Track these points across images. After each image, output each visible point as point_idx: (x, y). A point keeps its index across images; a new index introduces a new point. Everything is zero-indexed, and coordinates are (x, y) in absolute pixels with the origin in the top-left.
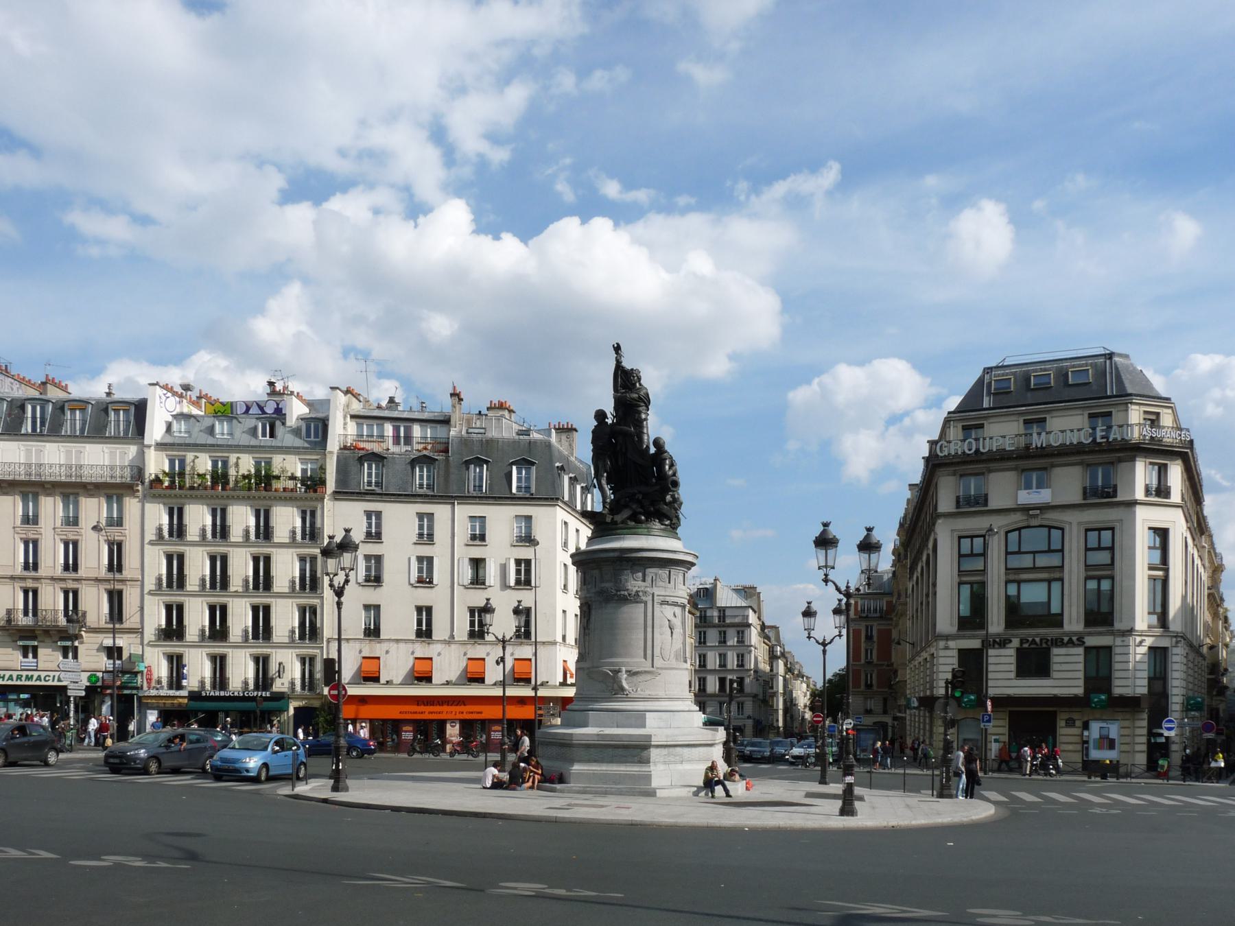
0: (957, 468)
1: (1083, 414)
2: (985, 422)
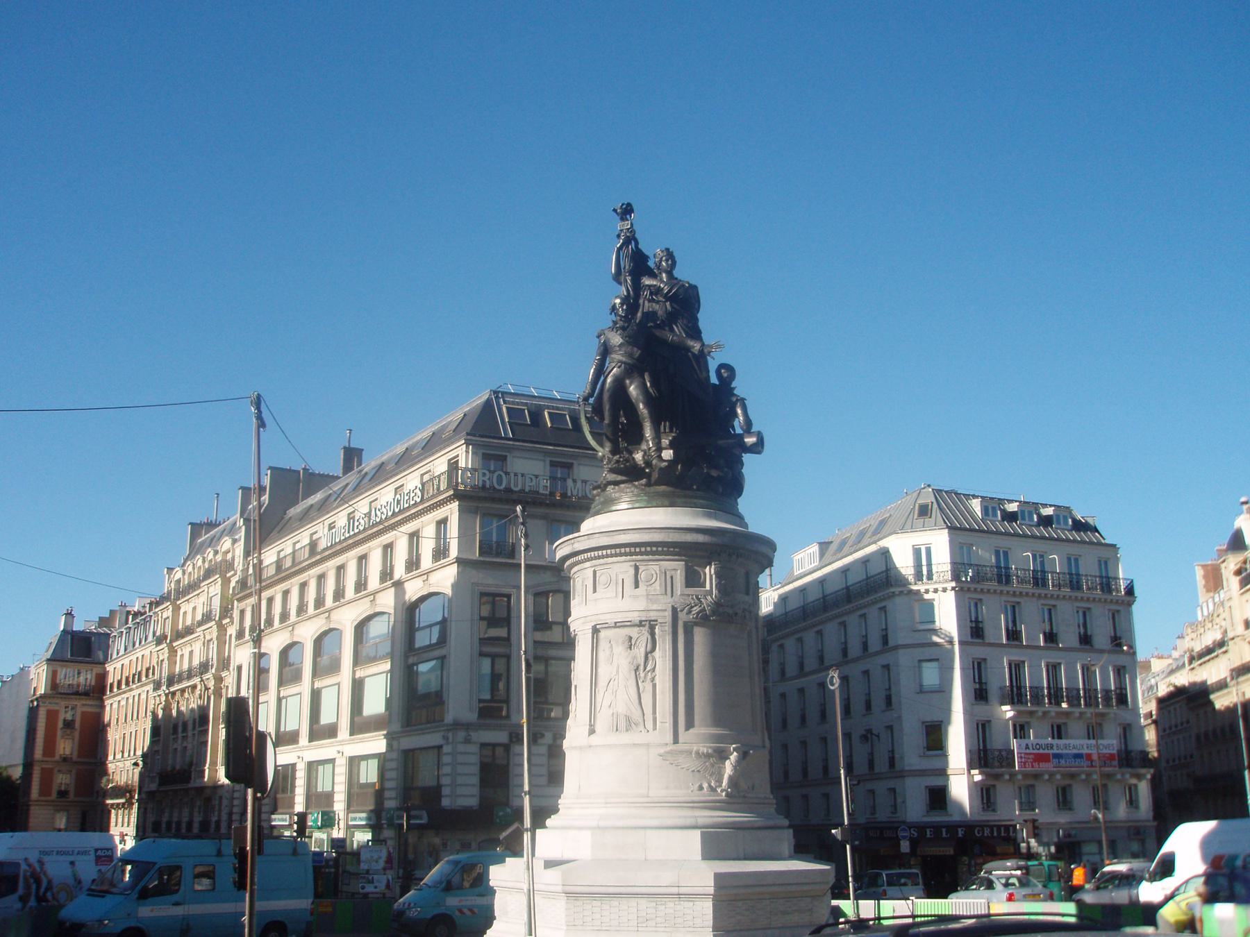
0: (480, 505)
1: (544, 461)
2: (507, 454)
